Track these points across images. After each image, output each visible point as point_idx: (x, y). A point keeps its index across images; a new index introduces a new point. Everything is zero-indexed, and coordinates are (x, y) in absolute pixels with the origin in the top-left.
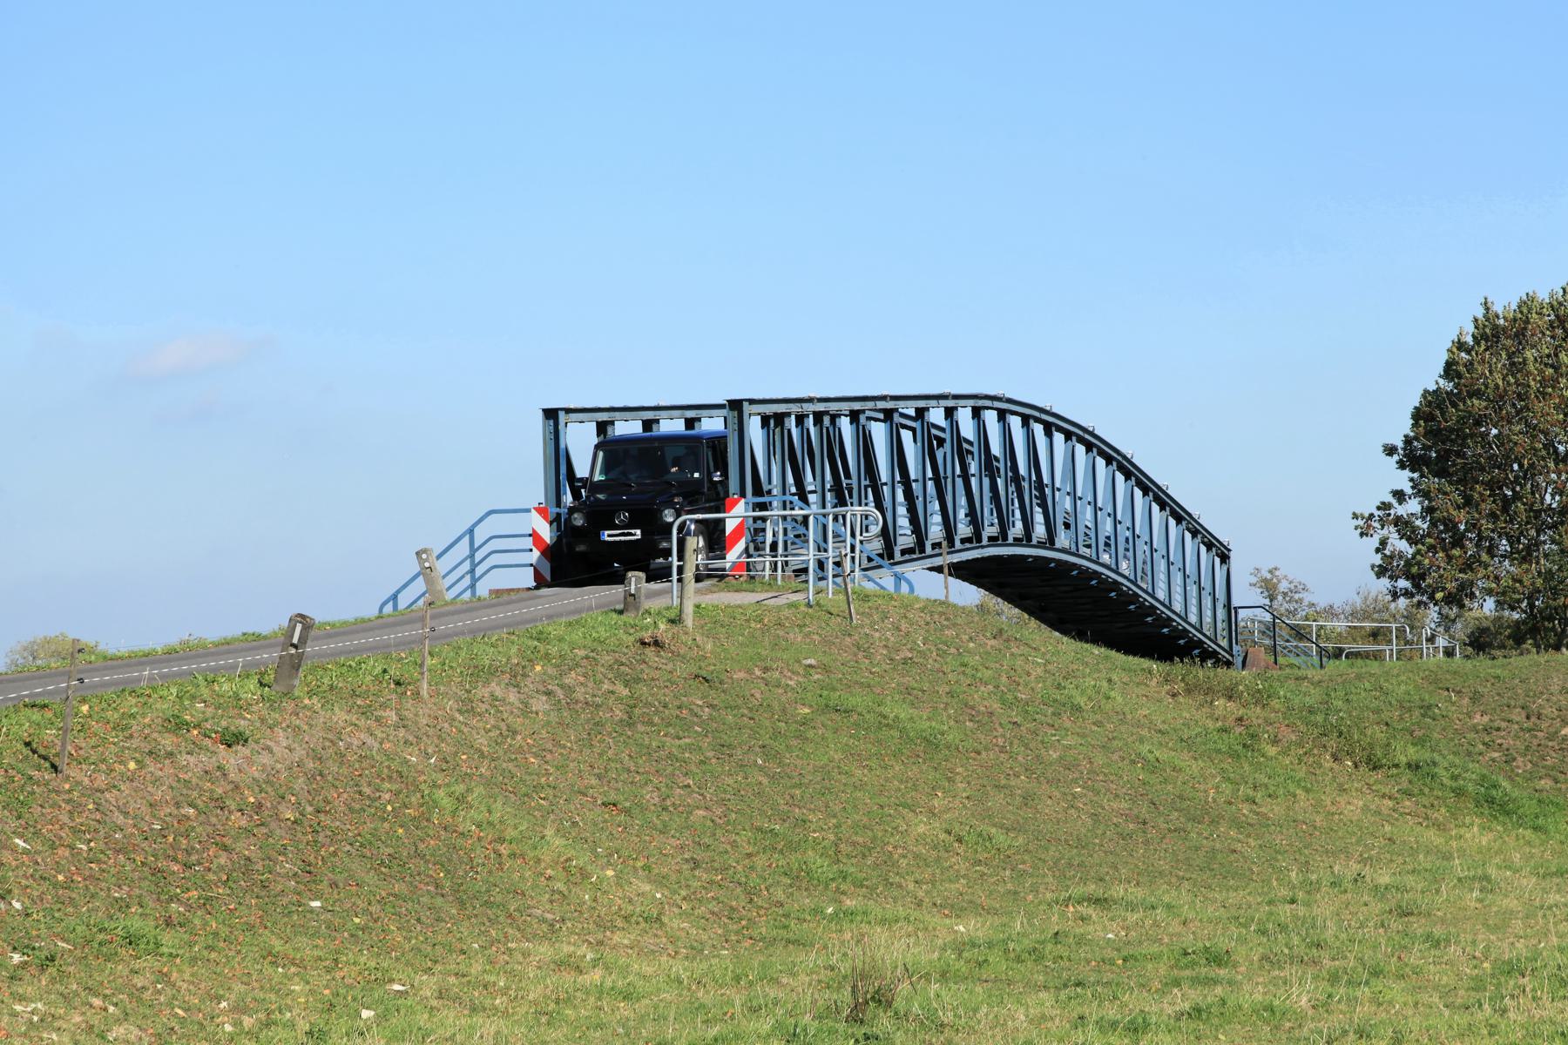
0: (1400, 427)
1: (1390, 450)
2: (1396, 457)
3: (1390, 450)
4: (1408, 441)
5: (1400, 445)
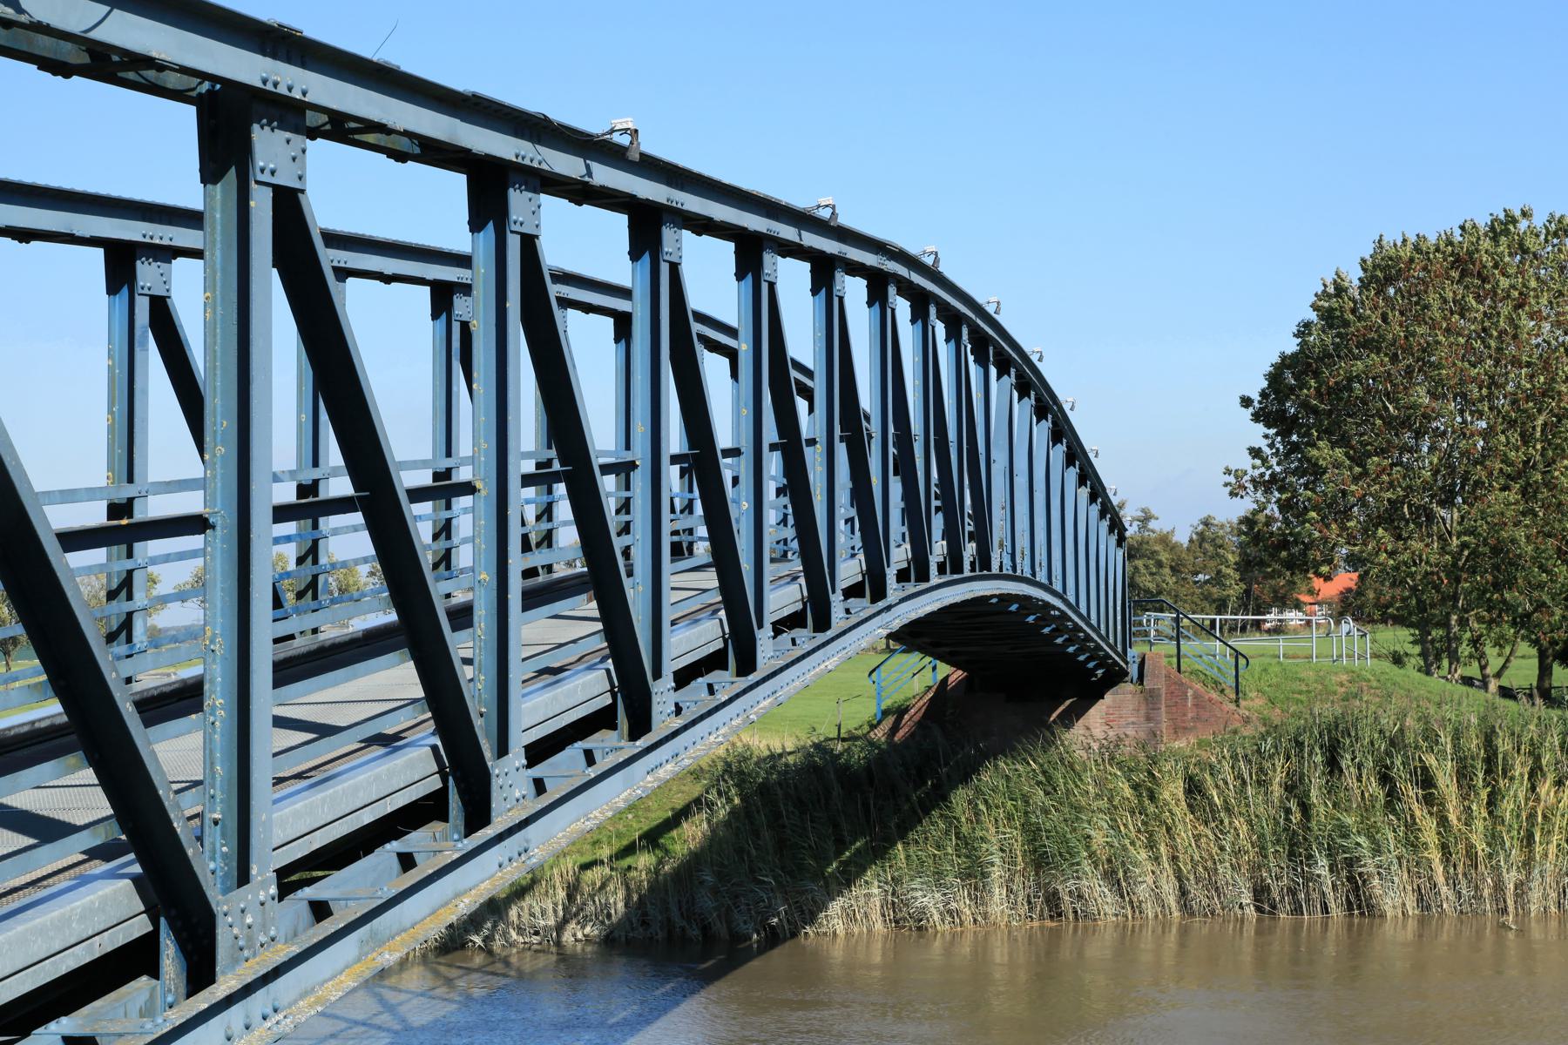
0: (1255, 385)
1: (1246, 402)
2: (1251, 410)
3: (1246, 402)
4: (1263, 394)
5: (1256, 397)
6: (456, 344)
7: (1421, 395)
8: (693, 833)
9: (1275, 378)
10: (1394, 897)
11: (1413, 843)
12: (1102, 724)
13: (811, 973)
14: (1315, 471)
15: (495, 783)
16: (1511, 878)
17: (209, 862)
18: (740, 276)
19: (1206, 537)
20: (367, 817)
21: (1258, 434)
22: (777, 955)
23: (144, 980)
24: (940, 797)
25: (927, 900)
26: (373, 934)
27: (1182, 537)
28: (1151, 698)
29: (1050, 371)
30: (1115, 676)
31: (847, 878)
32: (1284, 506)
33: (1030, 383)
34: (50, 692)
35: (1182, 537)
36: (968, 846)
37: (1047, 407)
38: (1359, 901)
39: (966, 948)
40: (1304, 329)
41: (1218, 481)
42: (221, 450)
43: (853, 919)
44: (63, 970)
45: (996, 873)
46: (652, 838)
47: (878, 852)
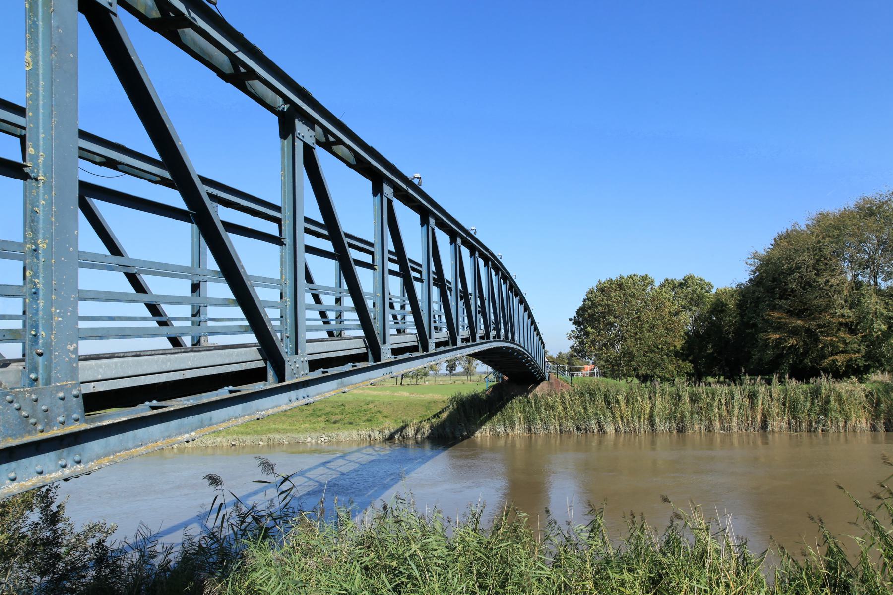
0: (574, 314)
1: (570, 320)
3: (570, 320)
6: (407, 355)
7: (611, 318)
8: (445, 415)
9: (578, 312)
10: (610, 429)
11: (614, 417)
12: (540, 390)
13: (474, 445)
14: (587, 334)
15: (382, 351)
16: (636, 425)
17: (285, 348)
18: (451, 244)
19: (560, 356)
20: (342, 353)
21: (574, 327)
22: (466, 442)
23: (263, 382)
24: (503, 405)
25: (500, 430)
26: (342, 383)
27: (555, 356)
28: (551, 384)
29: (527, 298)
30: (543, 379)
31: (482, 424)
32: (580, 343)
33: (523, 301)
34: (221, 275)
35: (555, 356)
36: (511, 418)
37: (527, 308)
38: (601, 429)
39: (510, 442)
40: (585, 301)
41: (565, 337)
42: (287, 222)
43: (483, 434)
44: (230, 371)
45: (517, 424)
46: (436, 415)
47: (489, 418)
